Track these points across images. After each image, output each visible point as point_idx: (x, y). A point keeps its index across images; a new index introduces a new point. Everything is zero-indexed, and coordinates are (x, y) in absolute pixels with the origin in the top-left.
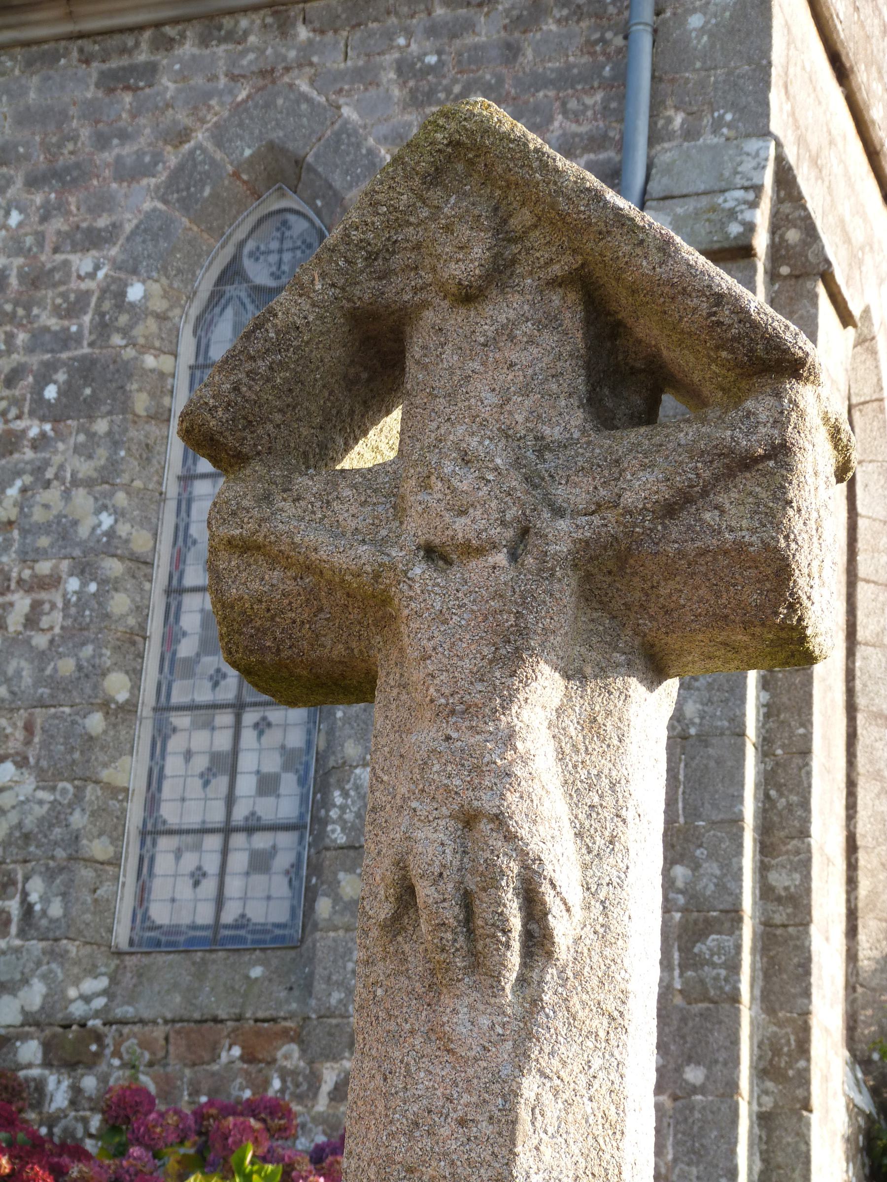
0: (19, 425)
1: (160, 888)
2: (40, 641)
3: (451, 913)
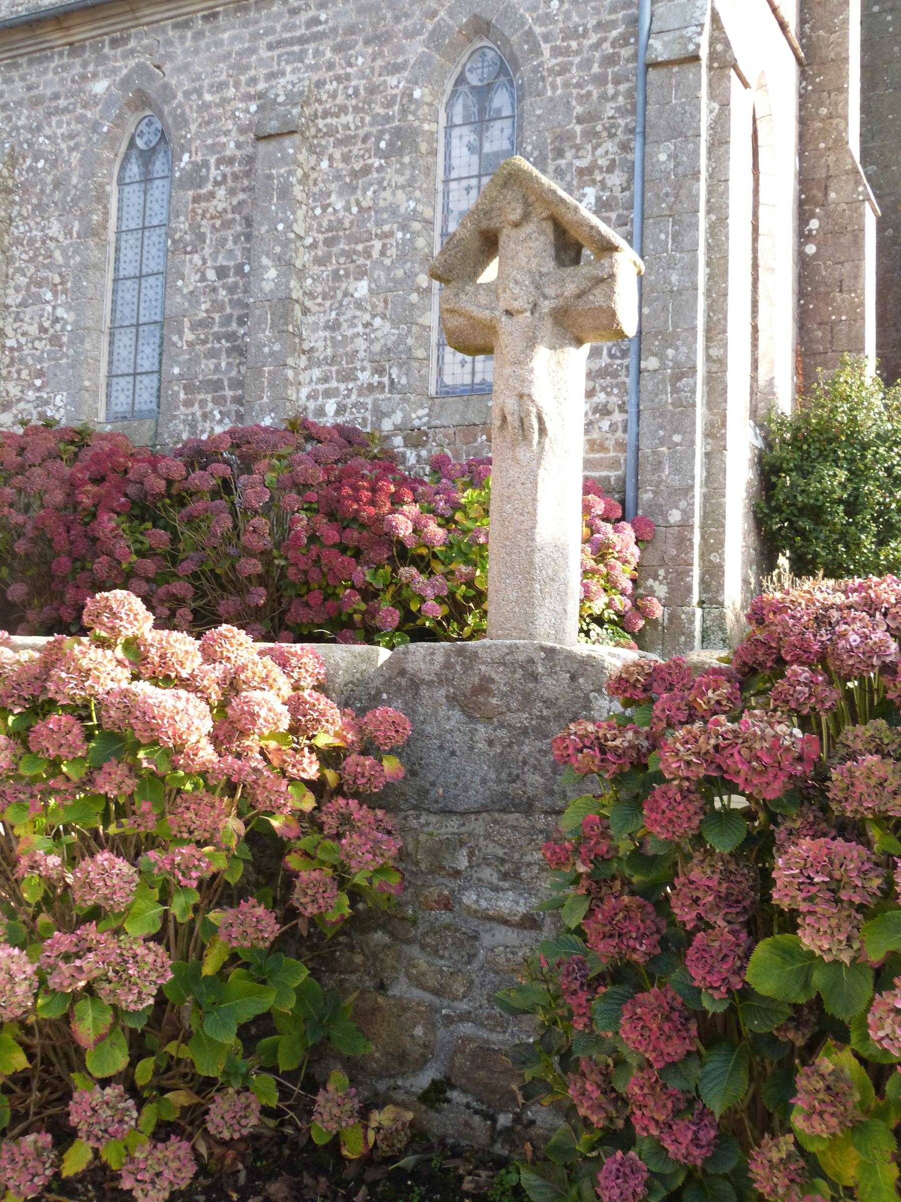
0: (370, 161)
1: (447, 369)
2: (387, 262)
3: (517, 424)
